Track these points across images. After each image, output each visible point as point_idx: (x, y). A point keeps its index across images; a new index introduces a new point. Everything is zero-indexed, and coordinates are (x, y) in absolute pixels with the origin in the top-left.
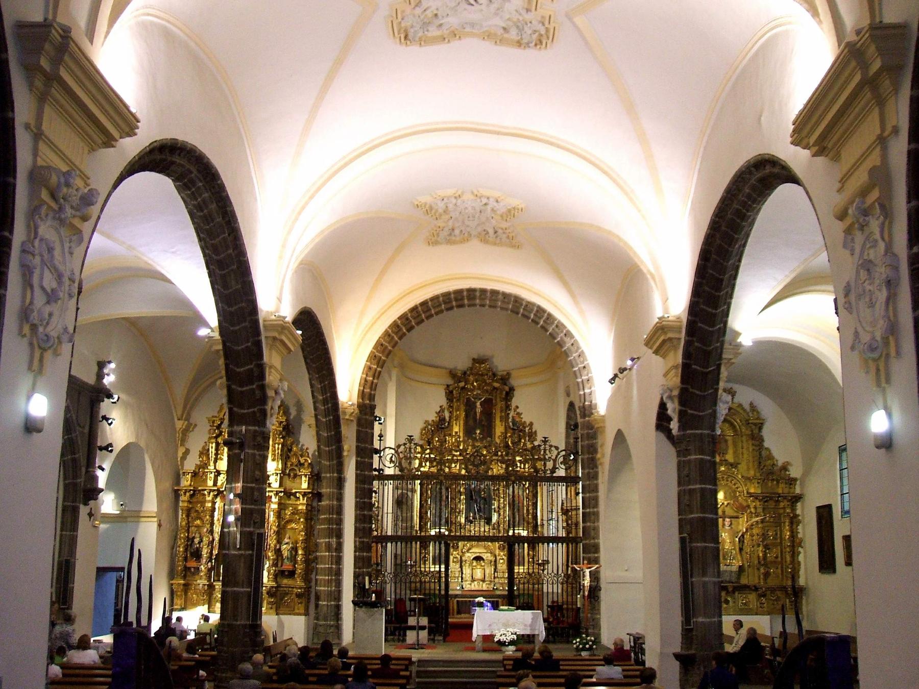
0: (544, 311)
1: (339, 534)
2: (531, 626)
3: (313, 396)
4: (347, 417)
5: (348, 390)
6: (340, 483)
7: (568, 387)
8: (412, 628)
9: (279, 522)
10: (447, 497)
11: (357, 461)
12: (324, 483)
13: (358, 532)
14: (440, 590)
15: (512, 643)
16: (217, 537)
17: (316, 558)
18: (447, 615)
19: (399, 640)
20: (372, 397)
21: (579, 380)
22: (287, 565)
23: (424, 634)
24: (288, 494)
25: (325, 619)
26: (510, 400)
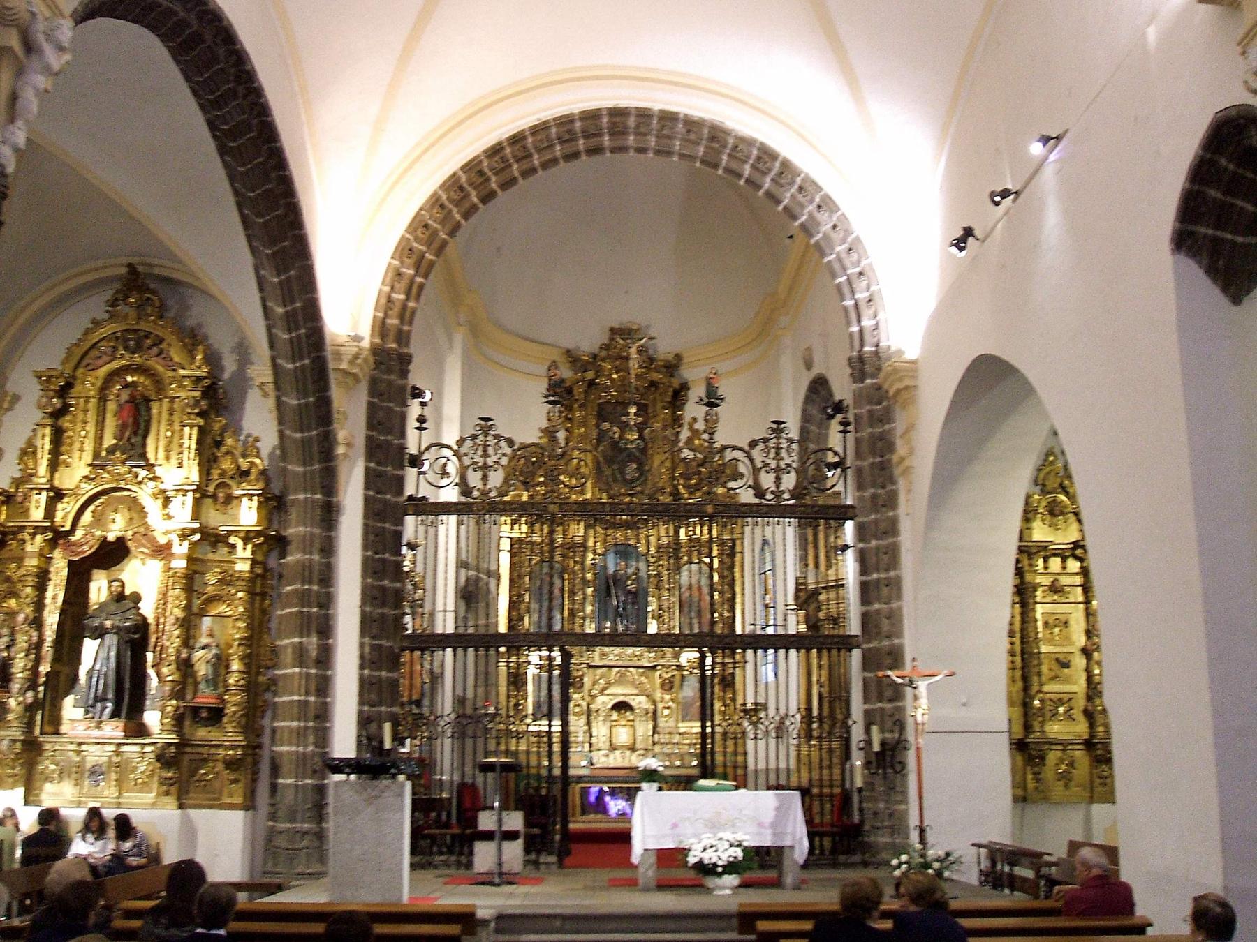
0: (774, 156)
1: (325, 628)
2: (774, 825)
3: (265, 307)
4: (344, 366)
5: (349, 304)
6: (329, 514)
7: (809, 349)
8: (488, 836)
9: (189, 599)
10: (562, 590)
11: (367, 469)
12: (293, 515)
13: (367, 624)
14: (550, 768)
15: (731, 868)
16: (50, 634)
17: (274, 681)
18: (563, 820)
19: (459, 865)
20: (403, 337)
21: (849, 303)
22: (205, 696)
23: (514, 852)
24: (213, 539)
25: (292, 819)
26: (681, 408)
